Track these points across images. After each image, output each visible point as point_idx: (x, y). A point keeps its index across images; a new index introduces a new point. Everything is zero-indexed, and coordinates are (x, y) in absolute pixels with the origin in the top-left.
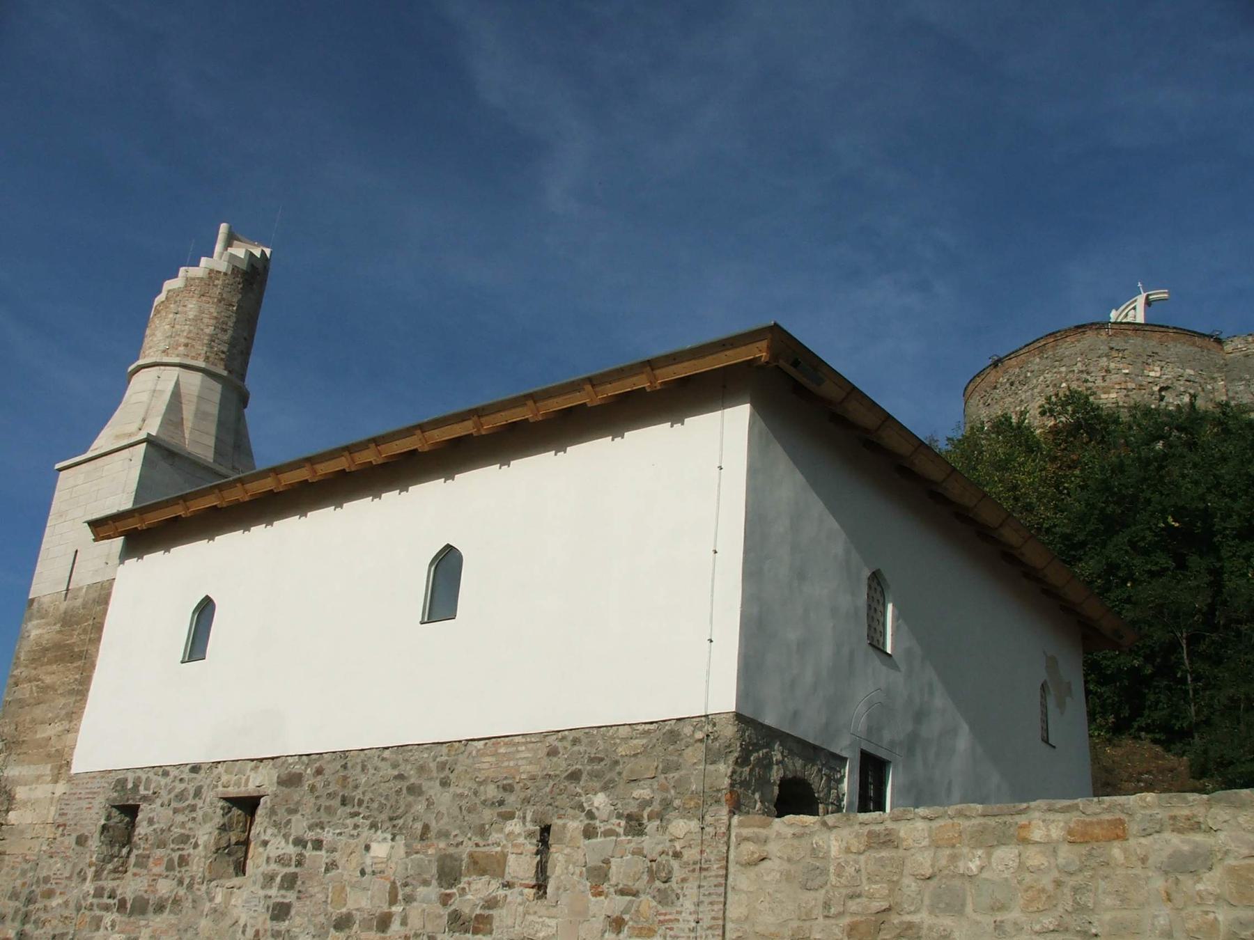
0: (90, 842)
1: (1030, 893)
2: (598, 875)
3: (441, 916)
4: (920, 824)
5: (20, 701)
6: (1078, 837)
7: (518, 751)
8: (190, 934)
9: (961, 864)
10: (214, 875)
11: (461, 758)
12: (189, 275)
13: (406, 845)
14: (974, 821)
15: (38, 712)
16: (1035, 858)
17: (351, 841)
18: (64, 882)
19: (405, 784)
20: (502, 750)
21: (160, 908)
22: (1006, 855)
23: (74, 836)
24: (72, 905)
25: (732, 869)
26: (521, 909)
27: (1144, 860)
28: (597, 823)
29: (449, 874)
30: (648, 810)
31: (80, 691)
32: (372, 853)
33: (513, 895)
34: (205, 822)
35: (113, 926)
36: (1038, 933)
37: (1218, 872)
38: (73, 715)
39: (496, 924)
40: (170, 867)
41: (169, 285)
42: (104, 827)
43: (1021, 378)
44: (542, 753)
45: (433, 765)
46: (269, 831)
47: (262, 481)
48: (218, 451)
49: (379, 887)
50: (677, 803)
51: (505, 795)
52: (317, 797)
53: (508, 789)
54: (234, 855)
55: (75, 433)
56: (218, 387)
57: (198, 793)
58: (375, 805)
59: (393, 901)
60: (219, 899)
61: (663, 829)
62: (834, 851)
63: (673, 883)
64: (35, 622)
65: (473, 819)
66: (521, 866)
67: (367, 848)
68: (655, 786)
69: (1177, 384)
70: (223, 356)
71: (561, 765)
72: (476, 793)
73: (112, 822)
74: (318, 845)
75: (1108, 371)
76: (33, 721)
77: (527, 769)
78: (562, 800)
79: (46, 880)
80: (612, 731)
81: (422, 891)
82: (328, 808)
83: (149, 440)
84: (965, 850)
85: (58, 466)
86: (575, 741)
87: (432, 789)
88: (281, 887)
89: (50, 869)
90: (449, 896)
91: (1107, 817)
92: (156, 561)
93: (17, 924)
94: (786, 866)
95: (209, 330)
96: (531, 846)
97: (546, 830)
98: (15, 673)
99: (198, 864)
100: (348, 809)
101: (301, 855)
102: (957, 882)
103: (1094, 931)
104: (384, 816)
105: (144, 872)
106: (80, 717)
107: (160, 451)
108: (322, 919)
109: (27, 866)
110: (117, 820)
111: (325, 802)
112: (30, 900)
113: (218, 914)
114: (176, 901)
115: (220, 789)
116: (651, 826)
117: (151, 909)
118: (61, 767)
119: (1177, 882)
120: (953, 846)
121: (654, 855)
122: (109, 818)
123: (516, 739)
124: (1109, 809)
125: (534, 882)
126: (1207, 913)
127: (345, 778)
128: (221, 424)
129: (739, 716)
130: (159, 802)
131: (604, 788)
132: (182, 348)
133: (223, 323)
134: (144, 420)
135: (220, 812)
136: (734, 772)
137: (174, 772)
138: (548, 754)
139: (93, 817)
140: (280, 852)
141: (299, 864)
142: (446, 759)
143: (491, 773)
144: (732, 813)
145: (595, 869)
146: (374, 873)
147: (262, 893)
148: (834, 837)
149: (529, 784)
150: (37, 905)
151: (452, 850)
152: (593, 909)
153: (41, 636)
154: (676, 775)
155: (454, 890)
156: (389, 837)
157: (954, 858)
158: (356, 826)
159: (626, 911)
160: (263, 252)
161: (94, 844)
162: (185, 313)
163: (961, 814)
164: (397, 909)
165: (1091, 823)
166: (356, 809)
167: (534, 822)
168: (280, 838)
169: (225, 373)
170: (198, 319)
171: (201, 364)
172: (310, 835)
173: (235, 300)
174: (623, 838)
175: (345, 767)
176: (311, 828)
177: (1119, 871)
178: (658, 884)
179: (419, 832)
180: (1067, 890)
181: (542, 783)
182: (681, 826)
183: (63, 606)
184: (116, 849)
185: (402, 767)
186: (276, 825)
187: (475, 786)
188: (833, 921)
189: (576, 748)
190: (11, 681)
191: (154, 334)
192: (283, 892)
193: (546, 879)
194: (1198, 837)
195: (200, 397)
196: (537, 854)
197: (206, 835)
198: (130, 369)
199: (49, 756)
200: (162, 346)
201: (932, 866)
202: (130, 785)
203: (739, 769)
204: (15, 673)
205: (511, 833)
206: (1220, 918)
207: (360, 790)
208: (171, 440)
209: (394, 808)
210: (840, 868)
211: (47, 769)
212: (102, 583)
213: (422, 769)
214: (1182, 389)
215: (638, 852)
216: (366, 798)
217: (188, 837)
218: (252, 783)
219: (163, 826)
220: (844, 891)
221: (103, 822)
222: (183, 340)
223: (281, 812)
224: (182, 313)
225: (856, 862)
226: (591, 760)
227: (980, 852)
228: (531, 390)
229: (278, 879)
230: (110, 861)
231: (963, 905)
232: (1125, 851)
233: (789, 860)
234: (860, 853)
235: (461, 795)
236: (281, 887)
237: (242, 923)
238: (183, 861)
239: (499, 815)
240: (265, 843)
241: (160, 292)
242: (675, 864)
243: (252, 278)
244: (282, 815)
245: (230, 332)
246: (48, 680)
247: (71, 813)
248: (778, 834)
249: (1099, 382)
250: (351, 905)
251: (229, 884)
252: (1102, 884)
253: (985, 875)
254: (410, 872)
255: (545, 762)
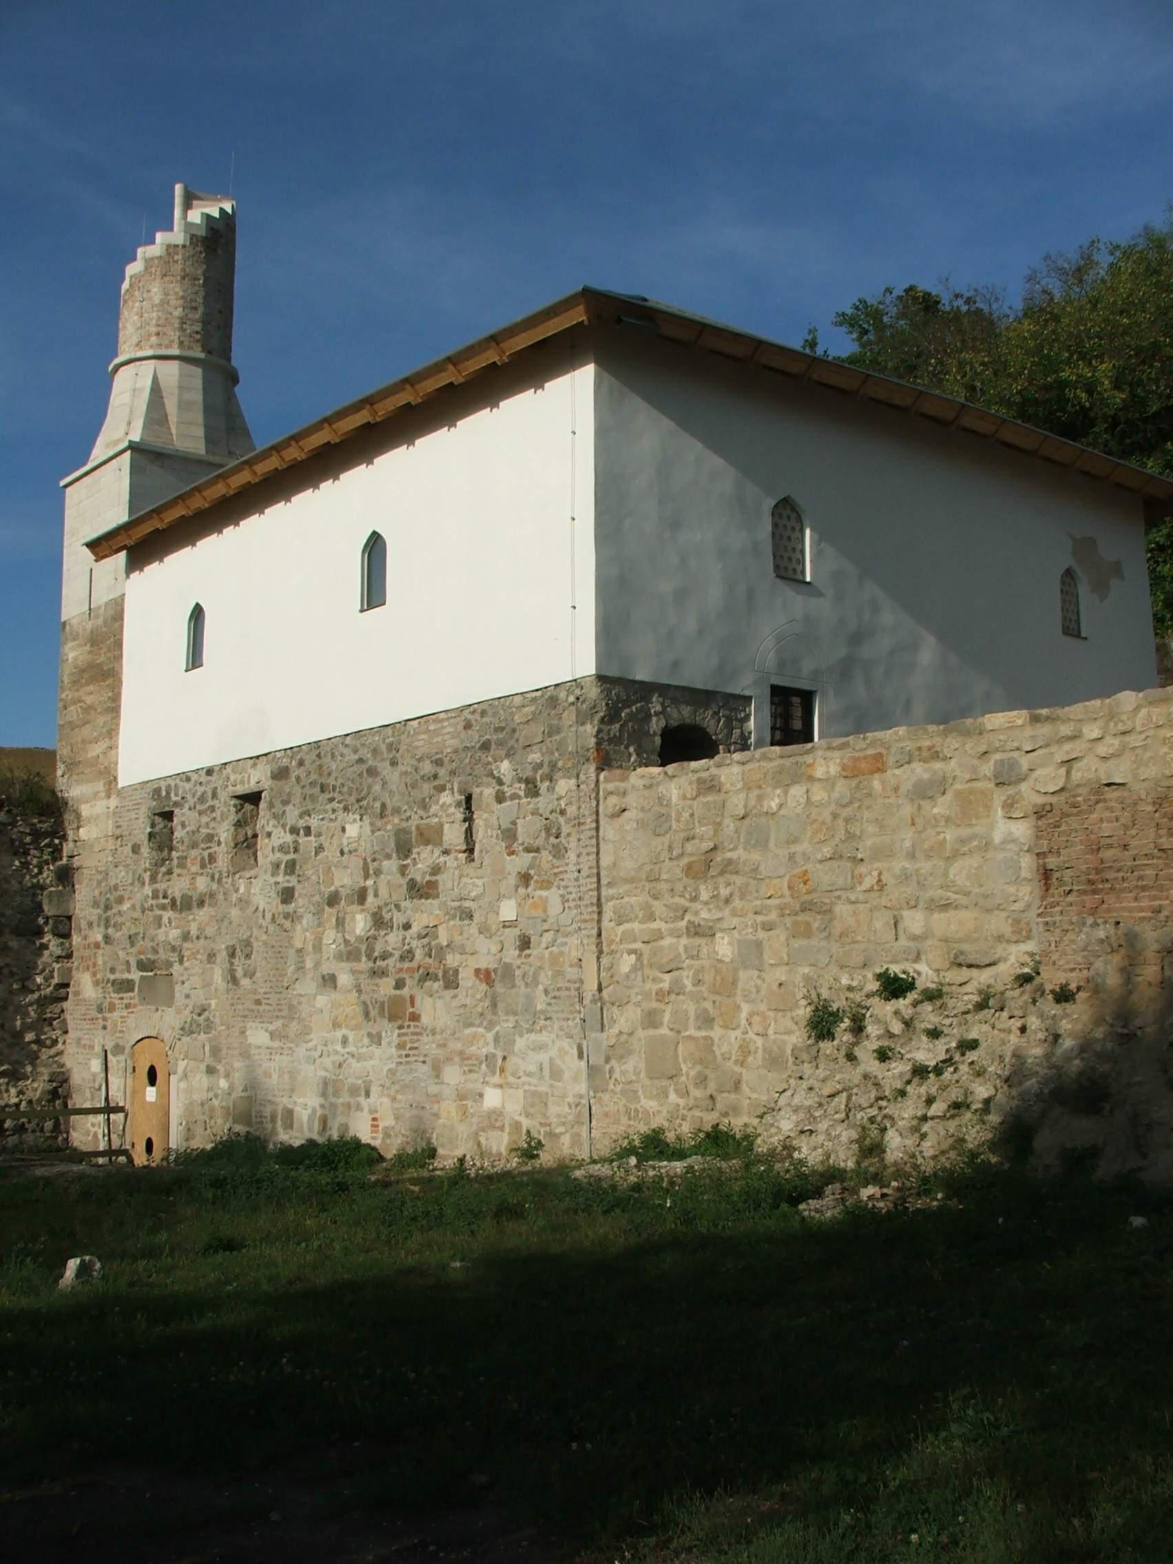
0: (142, 850)
1: (815, 826)
2: (509, 835)
3: (401, 886)
4: (736, 769)
5: (70, 722)
6: (851, 772)
7: (443, 727)
8: (226, 922)
9: (765, 803)
10: (237, 869)
11: (403, 737)
12: (148, 255)
13: (371, 824)
14: (776, 763)
15: (86, 732)
16: (819, 794)
17: (331, 824)
18: (130, 888)
19: (365, 767)
20: (432, 728)
21: (201, 903)
22: (797, 791)
23: (130, 845)
24: (138, 907)
25: (602, 822)
26: (457, 872)
27: (896, 789)
28: (505, 788)
29: (404, 849)
30: (540, 772)
31: (113, 708)
32: (347, 834)
33: (450, 861)
34: (223, 820)
35: (170, 922)
36: (821, 862)
37: (949, 796)
38: (112, 732)
39: (441, 888)
40: (203, 866)
41: (133, 269)
42: (151, 835)
44: (460, 727)
45: (383, 747)
46: (271, 823)
47: (214, 488)
48: (210, 440)
49: (355, 863)
50: (560, 764)
52: (303, 787)
53: (439, 763)
54: (246, 845)
55: (72, 450)
56: (199, 371)
57: (214, 796)
58: (345, 789)
59: (367, 877)
60: (242, 890)
61: (551, 789)
62: (674, 799)
63: (562, 839)
64: (70, 645)
65: (417, 794)
66: (453, 834)
67: (344, 830)
68: (544, 750)
70: (198, 337)
71: (474, 738)
72: (416, 770)
73: (157, 829)
74: (308, 831)
76: (83, 741)
77: (452, 743)
78: (479, 769)
79: (116, 888)
81: (386, 863)
82: (312, 796)
83: (132, 447)
84: (769, 790)
85: (62, 483)
86: (483, 713)
87: (385, 768)
88: (286, 874)
89: (117, 878)
90: (405, 866)
91: (870, 752)
92: (153, 569)
93: (102, 929)
94: (641, 815)
95: (178, 312)
96: (459, 815)
97: (469, 799)
98: (63, 696)
99: (223, 863)
100: (327, 796)
101: (296, 842)
102: (763, 820)
103: (860, 856)
104: (353, 799)
105: (184, 872)
106: (118, 734)
107: (147, 456)
108: (317, 898)
109: (100, 877)
110: (161, 826)
111: (308, 791)
112: (107, 908)
113: (243, 902)
114: (212, 895)
115: (230, 788)
116: (544, 787)
117: (195, 904)
118: (110, 782)
119: (919, 807)
120: (760, 787)
121: (547, 815)
122: (153, 825)
123: (442, 716)
124: (872, 744)
125: (464, 848)
126: (939, 833)
127: (320, 767)
128: (208, 409)
129: (601, 678)
130: (187, 806)
131: (508, 756)
132: (154, 339)
133: (191, 300)
134: (129, 423)
135: (233, 809)
136: (599, 731)
137: (194, 777)
138: (465, 728)
139: (141, 828)
140: (281, 841)
141: (296, 850)
142: (389, 741)
144: (600, 769)
145: (508, 830)
146: (350, 852)
147: (272, 880)
148: (677, 783)
150: (114, 911)
151: (404, 825)
152: (509, 868)
153: (76, 658)
154: (557, 737)
155: (409, 861)
156: (358, 817)
157: (760, 798)
158: (334, 811)
159: (531, 867)
160: (222, 210)
161: (145, 850)
162: (151, 299)
163: (764, 757)
164: (370, 883)
165: (858, 759)
166: (332, 795)
167: (460, 792)
168: (280, 829)
169: (202, 356)
170: (165, 302)
171: (176, 351)
172: (301, 824)
173: (200, 272)
174: (524, 800)
175: (319, 756)
176: (301, 816)
177: (880, 801)
178: (553, 840)
179: (379, 811)
180: (840, 822)
181: (463, 755)
182: (564, 785)
183: (89, 626)
184: (166, 852)
185: (361, 752)
186: (275, 816)
187: (415, 763)
188: (675, 863)
189: (484, 720)
190: (61, 705)
191: (124, 327)
192: (287, 877)
194: (937, 766)
195: (181, 387)
196: (465, 821)
197: (225, 832)
198: (110, 368)
199: (100, 773)
200: (135, 339)
201: (745, 806)
202: (164, 794)
203: (605, 728)
204: (63, 696)
205: (444, 804)
206: (948, 837)
207: (332, 777)
208: (158, 443)
209: (359, 791)
210: (679, 814)
211: (100, 786)
212: (115, 599)
216: (338, 784)
217: (213, 836)
218: (258, 778)
219: (193, 828)
220: (683, 835)
221: (149, 830)
222: (154, 330)
223: (278, 803)
224: (150, 295)
225: (691, 807)
227: (778, 791)
228: (155, 506)
229: (283, 866)
230: (163, 865)
231: (767, 841)
232: (883, 782)
233: (642, 809)
234: (694, 799)
235: (406, 773)
236: (286, 874)
237: (261, 908)
238: (212, 858)
239: (435, 788)
240: (269, 835)
241: (123, 279)
242: (562, 820)
243: (216, 242)
244: (278, 808)
245: (201, 310)
246: (89, 700)
247: (125, 825)
248: (633, 787)
250: (337, 883)
251: (248, 876)
252: (866, 814)
253: (782, 812)
254: (376, 848)
255: (463, 735)
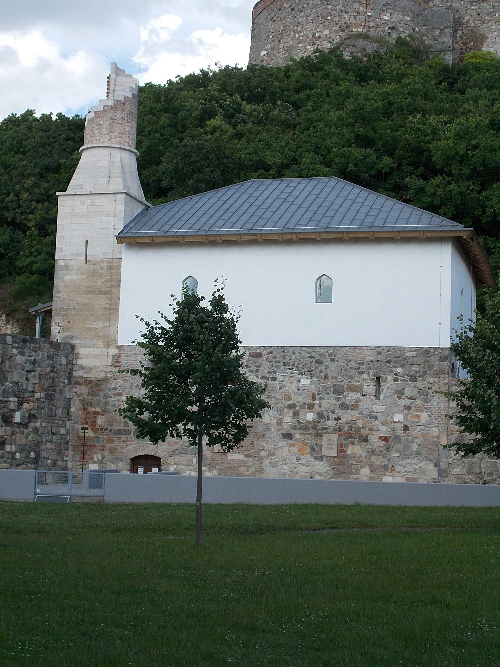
2: (400, 394)
43: (300, 7)
50: (428, 372)
51: (360, 366)
67: (299, 381)
69: (399, 26)
71: (383, 357)
74: (274, 379)
75: (358, 13)
80: (403, 349)
97: (378, 379)
142: (332, 353)
143: (353, 358)
149: (370, 363)
156: (309, 378)
159: (412, 404)
167: (373, 375)
193: (380, 394)
207: (292, 361)
213: (321, 355)
214: (402, 30)
215: (415, 387)
216: (296, 364)
226: (395, 357)
239: (358, 372)
249: (352, 20)
